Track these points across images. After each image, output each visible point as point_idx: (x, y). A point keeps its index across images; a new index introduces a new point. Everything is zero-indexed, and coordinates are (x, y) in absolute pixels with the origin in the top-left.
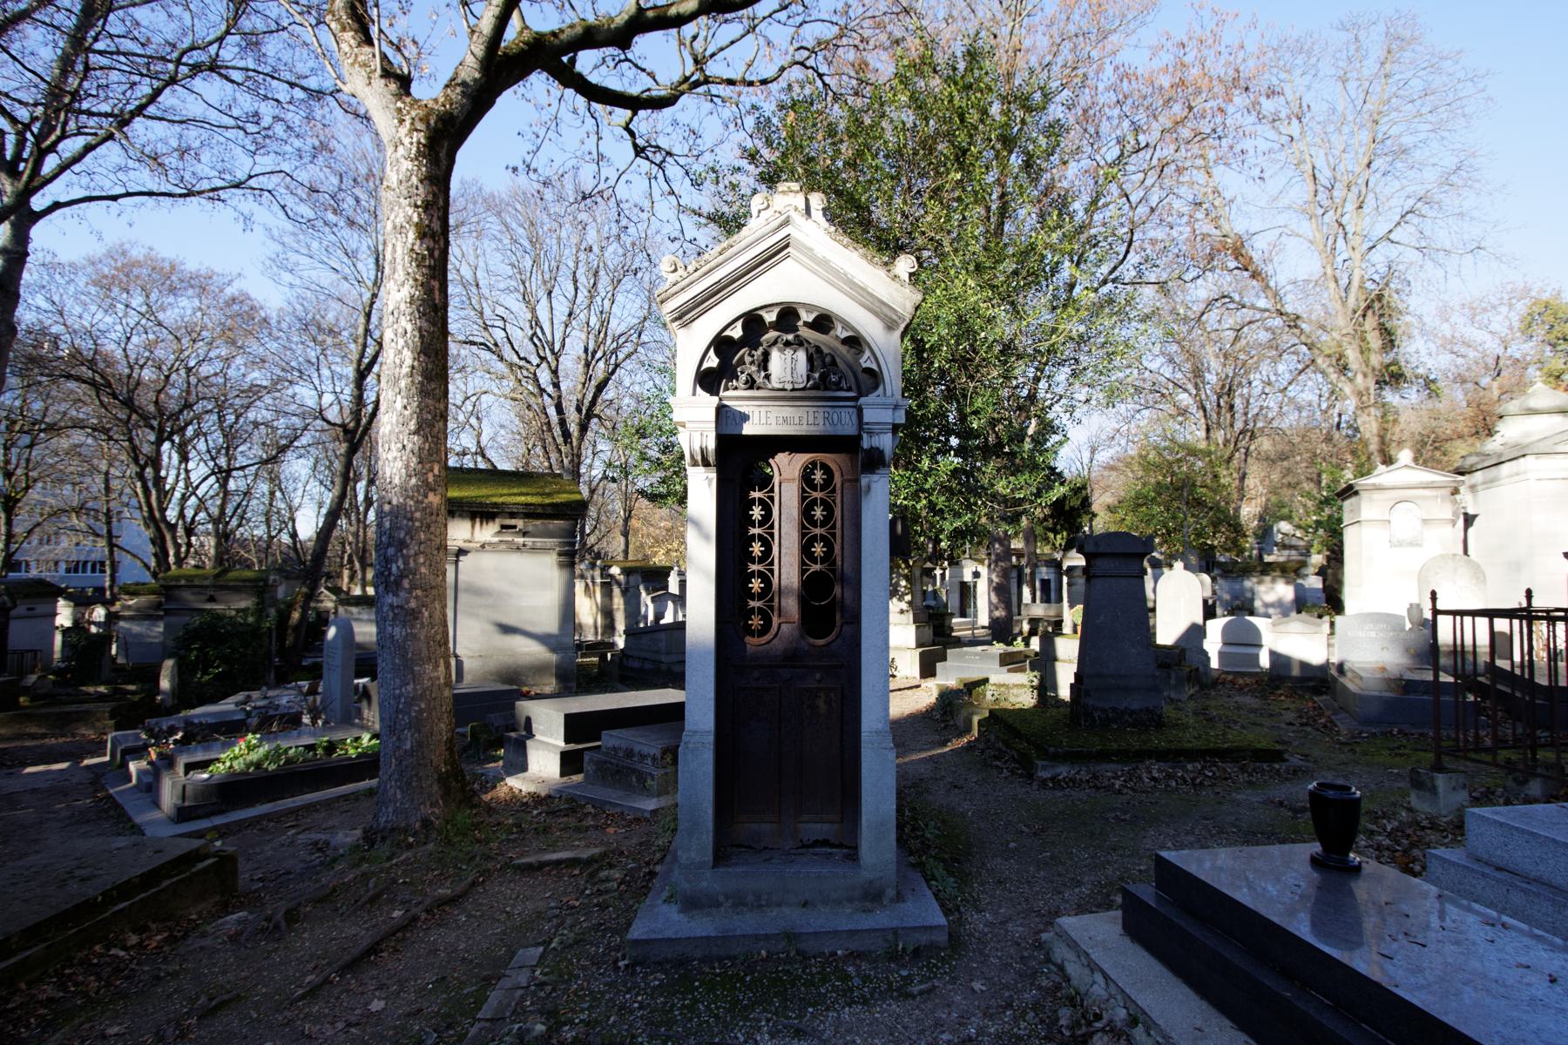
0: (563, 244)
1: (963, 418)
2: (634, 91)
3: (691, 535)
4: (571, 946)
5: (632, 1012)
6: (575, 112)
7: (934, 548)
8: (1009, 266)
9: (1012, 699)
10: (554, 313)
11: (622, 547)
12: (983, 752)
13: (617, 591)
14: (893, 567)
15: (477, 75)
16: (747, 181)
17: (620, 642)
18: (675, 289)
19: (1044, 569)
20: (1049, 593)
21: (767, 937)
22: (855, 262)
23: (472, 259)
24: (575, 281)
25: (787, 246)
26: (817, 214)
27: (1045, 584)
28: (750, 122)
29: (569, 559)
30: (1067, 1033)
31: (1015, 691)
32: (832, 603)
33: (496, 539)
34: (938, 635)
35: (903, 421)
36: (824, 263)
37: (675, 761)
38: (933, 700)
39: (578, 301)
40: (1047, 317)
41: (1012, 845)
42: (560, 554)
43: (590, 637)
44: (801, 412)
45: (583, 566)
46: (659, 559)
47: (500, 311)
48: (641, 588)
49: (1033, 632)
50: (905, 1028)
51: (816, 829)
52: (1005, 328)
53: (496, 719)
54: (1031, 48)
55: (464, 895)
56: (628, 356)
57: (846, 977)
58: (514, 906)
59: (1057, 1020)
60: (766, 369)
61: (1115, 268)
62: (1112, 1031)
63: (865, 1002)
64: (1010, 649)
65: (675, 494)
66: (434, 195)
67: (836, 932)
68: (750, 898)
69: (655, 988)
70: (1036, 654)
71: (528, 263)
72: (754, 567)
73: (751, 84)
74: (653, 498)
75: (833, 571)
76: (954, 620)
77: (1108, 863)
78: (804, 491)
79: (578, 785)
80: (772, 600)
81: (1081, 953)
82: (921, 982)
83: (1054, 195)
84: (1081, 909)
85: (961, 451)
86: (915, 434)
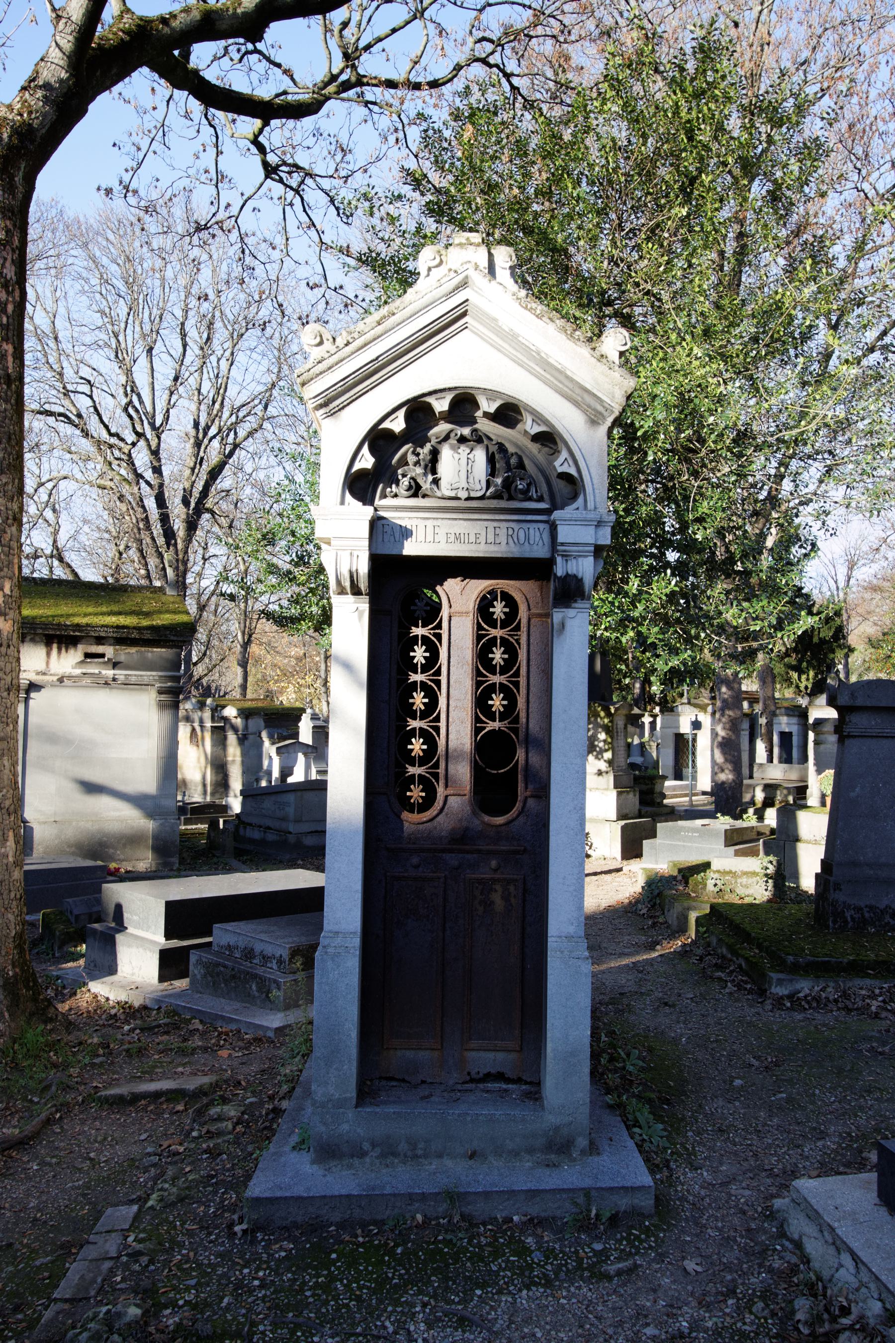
0: (169, 286)
1: (684, 526)
2: (265, 92)
3: (337, 678)
4: (173, 1204)
5: (251, 1291)
6: (187, 116)
7: (643, 688)
8: (748, 328)
9: (741, 891)
10: (154, 376)
11: (239, 680)
12: (701, 959)
13: (232, 738)
14: (593, 715)
15: (64, 75)
16: (411, 213)
17: (236, 805)
18: (321, 367)
19: (784, 719)
20: (789, 750)
21: (424, 1197)
22: (547, 335)
23: (49, 304)
24: (184, 335)
25: (464, 314)
26: (503, 274)
27: (785, 737)
28: (414, 134)
29: (175, 693)
30: (806, 1331)
31: (744, 880)
32: (512, 769)
33: (78, 671)
34: (645, 806)
35: (608, 541)
36: (512, 337)
37: (309, 965)
38: (639, 889)
39: (187, 361)
40: (792, 395)
41: (738, 1082)
42: (160, 692)
43: (197, 797)
44: (479, 527)
45: (188, 705)
46: (288, 698)
47: (85, 372)
48: (264, 735)
49: (768, 802)
50: (599, 1318)
51: (486, 1059)
52: (740, 409)
53: (75, 905)
54: (782, 39)
55: (36, 1135)
56: (250, 434)
57: (523, 1251)
58: (99, 1152)
59: (793, 1312)
60: (434, 471)
61: (885, 333)
62: (863, 1329)
63: (548, 1283)
64: (739, 824)
65: (311, 617)
66: (8, 231)
67: (512, 1193)
68: (403, 1147)
69: (280, 1261)
70: (773, 832)
71: (122, 310)
72: (415, 724)
73: (417, 86)
74: (282, 621)
75: (516, 731)
76: (668, 783)
77: (861, 1108)
78: (480, 628)
79: (181, 994)
80: (436, 766)
81: (824, 1227)
82: (619, 1259)
83: (807, 236)
84: (825, 1170)
85: (681, 570)
86: (620, 553)
